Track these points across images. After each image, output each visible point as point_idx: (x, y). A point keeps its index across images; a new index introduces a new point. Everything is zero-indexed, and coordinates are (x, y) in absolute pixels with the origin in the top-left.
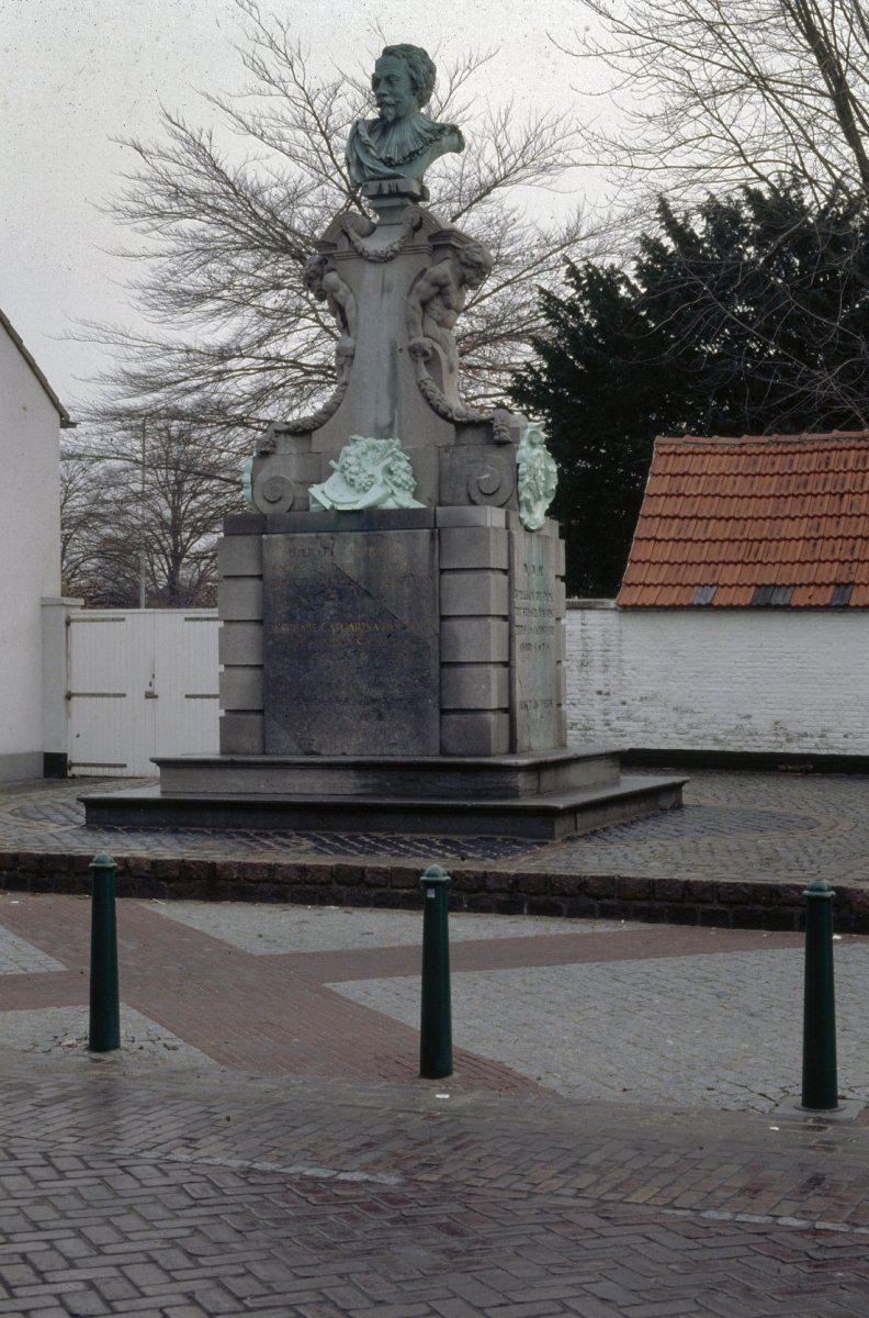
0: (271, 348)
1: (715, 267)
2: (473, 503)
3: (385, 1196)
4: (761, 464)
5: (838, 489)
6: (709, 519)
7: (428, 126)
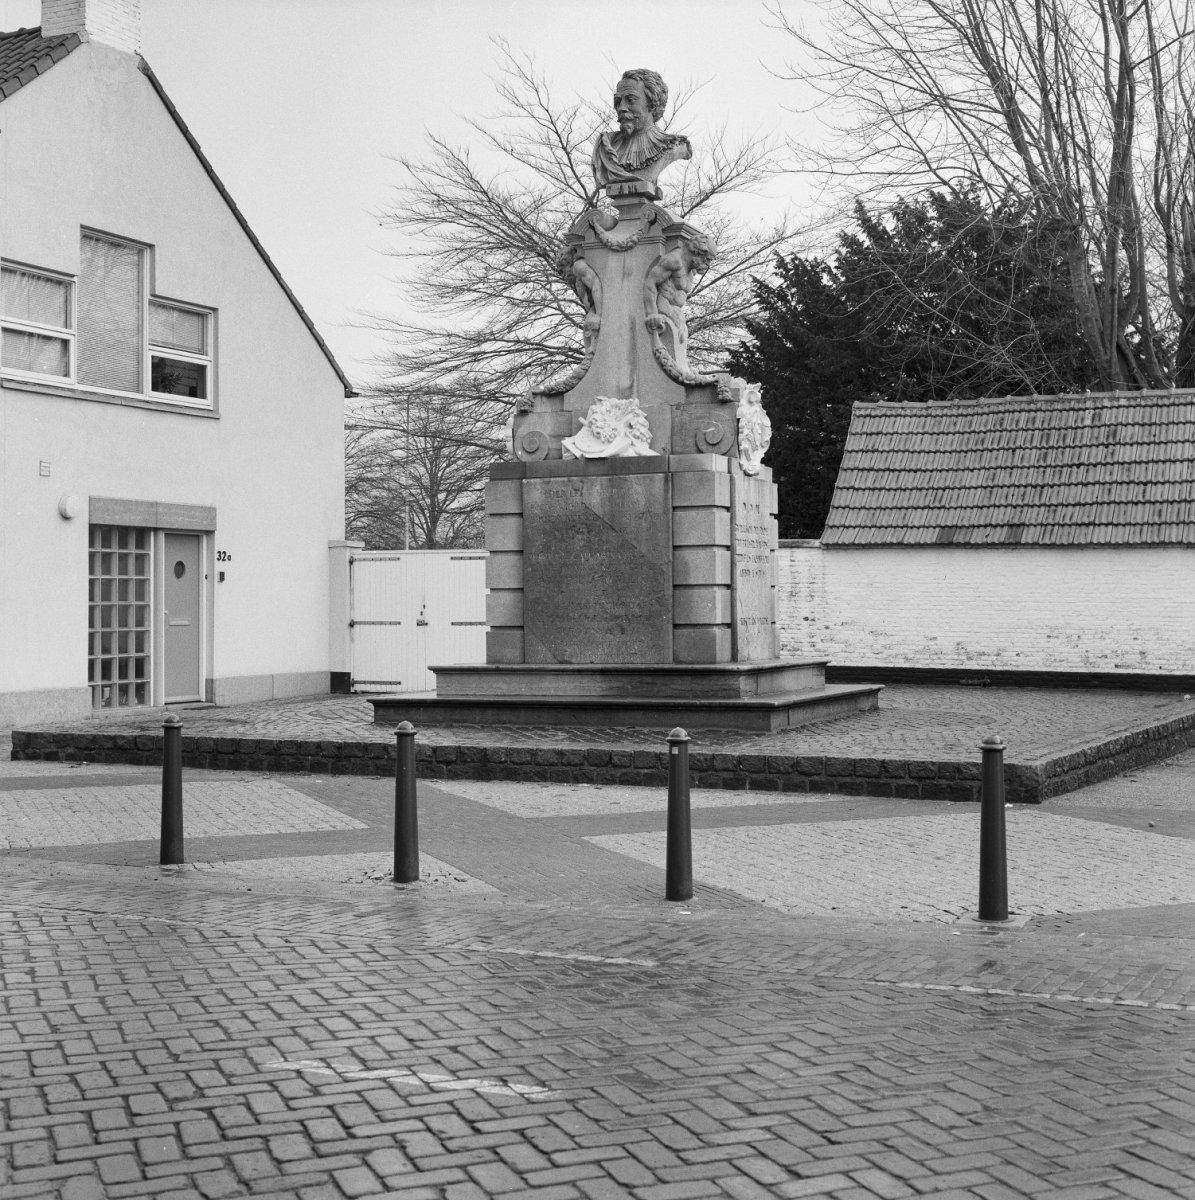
0: (522, 333)
1: (901, 259)
2: (700, 451)
3: (645, 973)
4: (945, 424)
5: (1011, 445)
6: (900, 471)
7: (661, 137)
